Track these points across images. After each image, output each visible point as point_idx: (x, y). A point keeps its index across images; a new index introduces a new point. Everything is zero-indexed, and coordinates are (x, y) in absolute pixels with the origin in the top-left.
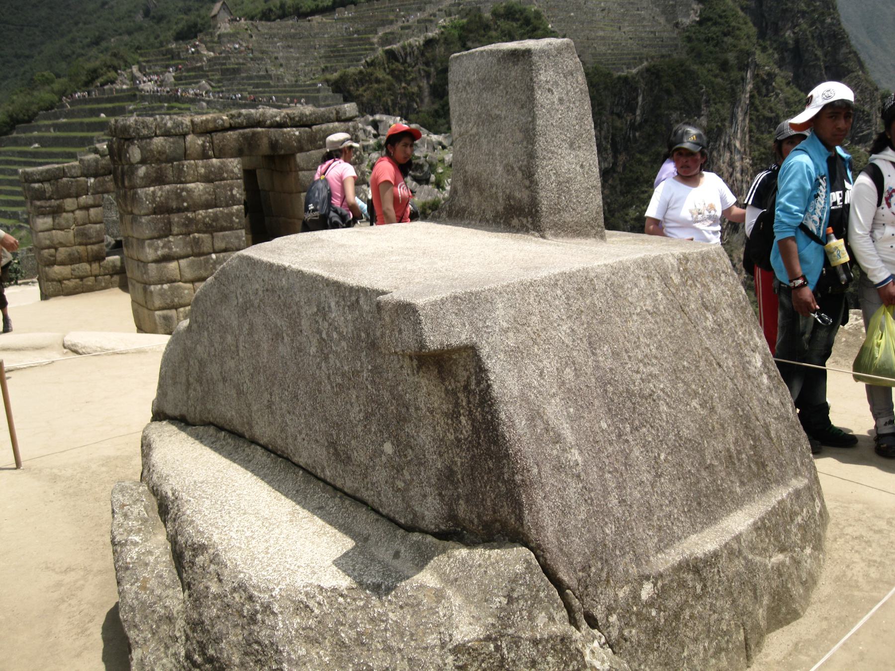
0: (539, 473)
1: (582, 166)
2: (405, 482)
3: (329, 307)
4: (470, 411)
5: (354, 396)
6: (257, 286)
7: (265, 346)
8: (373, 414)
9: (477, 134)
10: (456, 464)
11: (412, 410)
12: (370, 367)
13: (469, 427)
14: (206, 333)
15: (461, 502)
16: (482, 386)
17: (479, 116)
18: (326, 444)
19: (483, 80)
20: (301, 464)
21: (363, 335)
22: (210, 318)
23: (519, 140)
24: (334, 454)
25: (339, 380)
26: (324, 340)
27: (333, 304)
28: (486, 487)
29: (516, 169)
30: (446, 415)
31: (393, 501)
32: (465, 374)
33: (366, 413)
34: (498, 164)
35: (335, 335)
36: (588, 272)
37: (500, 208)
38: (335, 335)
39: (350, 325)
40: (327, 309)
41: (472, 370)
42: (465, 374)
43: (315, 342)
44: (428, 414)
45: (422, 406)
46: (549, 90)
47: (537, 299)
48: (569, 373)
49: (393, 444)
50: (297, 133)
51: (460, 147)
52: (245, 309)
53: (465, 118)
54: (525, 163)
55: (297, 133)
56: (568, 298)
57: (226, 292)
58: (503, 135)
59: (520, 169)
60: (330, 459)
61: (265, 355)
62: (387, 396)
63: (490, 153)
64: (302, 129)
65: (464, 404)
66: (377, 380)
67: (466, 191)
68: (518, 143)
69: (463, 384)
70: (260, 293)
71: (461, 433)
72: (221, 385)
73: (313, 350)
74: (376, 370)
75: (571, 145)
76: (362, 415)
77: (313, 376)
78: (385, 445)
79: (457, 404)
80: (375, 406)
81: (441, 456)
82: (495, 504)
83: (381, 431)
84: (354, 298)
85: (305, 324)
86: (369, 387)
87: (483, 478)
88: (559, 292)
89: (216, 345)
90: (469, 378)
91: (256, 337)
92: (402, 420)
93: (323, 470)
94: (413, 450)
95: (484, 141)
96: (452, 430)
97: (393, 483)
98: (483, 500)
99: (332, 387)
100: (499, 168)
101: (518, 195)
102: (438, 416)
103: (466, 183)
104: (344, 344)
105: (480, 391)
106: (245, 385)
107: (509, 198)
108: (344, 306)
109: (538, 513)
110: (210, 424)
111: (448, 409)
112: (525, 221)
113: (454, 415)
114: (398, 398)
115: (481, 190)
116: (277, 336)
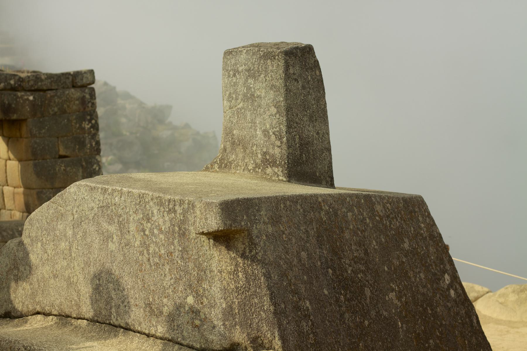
0: (285, 308)
1: (318, 133)
2: (201, 320)
3: (152, 213)
4: (245, 269)
5: (167, 270)
6: (93, 205)
7: (96, 245)
8: (180, 279)
9: (243, 108)
10: (235, 303)
11: (208, 272)
12: (180, 249)
13: (244, 279)
14: (39, 244)
15: (238, 327)
16: (252, 253)
17: (245, 95)
18: (144, 306)
19: (249, 70)
20: (122, 325)
21: (177, 229)
22: (44, 232)
23: (274, 113)
24: (149, 312)
25: (157, 260)
26: (147, 235)
27: (155, 212)
28: (253, 315)
29: (271, 134)
30: (230, 273)
31: (192, 334)
32: (243, 246)
33: (176, 279)
34: (258, 130)
35: (156, 231)
36: (318, 198)
37: (258, 161)
38: (156, 231)
39: (168, 224)
40: (150, 215)
41: (247, 244)
42: (243, 246)
43: (139, 238)
44: (219, 274)
45: (214, 269)
46: (296, 80)
47: (285, 209)
48: (304, 254)
49: (194, 297)
50: (31, 98)
51: (230, 117)
52: (77, 224)
53: (234, 96)
54: (278, 129)
55: (31, 98)
56: (304, 211)
57: (63, 211)
58: (262, 110)
59: (274, 133)
60: (146, 315)
61: (96, 252)
62: (191, 265)
63: (253, 122)
64: (37, 94)
65: (241, 265)
66: (185, 256)
67: (233, 149)
68: (272, 115)
69: (241, 252)
70: (96, 209)
71: (239, 283)
72: (52, 281)
73: (138, 243)
74: (185, 250)
75: (311, 118)
76: (172, 281)
77: (137, 261)
78: (188, 298)
79: (237, 265)
80: (182, 273)
81: (225, 299)
82: (258, 326)
83: (186, 290)
84: (171, 206)
85: (132, 227)
86: (179, 262)
87: (251, 310)
88: (299, 207)
89: (49, 252)
90: (245, 248)
91: (89, 240)
92: (200, 280)
93: (140, 324)
94: (207, 299)
95: (248, 114)
96: (233, 282)
97: (193, 323)
98: (251, 324)
99: (151, 266)
100: (259, 132)
101: (271, 151)
102: (224, 274)
103: (233, 143)
104: (162, 236)
105: (251, 256)
106: (75, 278)
107: (265, 154)
108: (164, 211)
109: (284, 331)
110: (38, 313)
111: (231, 269)
112: (276, 170)
113: (235, 272)
114: (199, 267)
115: (245, 148)
116: (107, 238)
